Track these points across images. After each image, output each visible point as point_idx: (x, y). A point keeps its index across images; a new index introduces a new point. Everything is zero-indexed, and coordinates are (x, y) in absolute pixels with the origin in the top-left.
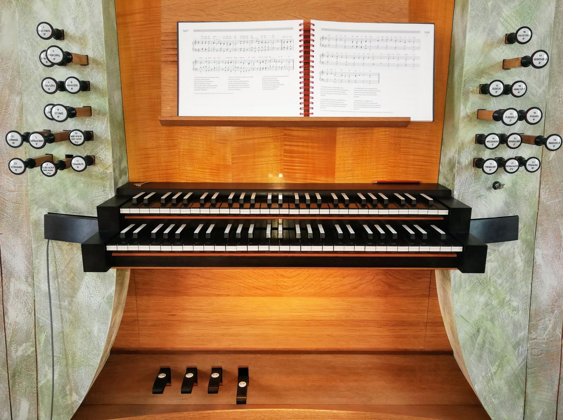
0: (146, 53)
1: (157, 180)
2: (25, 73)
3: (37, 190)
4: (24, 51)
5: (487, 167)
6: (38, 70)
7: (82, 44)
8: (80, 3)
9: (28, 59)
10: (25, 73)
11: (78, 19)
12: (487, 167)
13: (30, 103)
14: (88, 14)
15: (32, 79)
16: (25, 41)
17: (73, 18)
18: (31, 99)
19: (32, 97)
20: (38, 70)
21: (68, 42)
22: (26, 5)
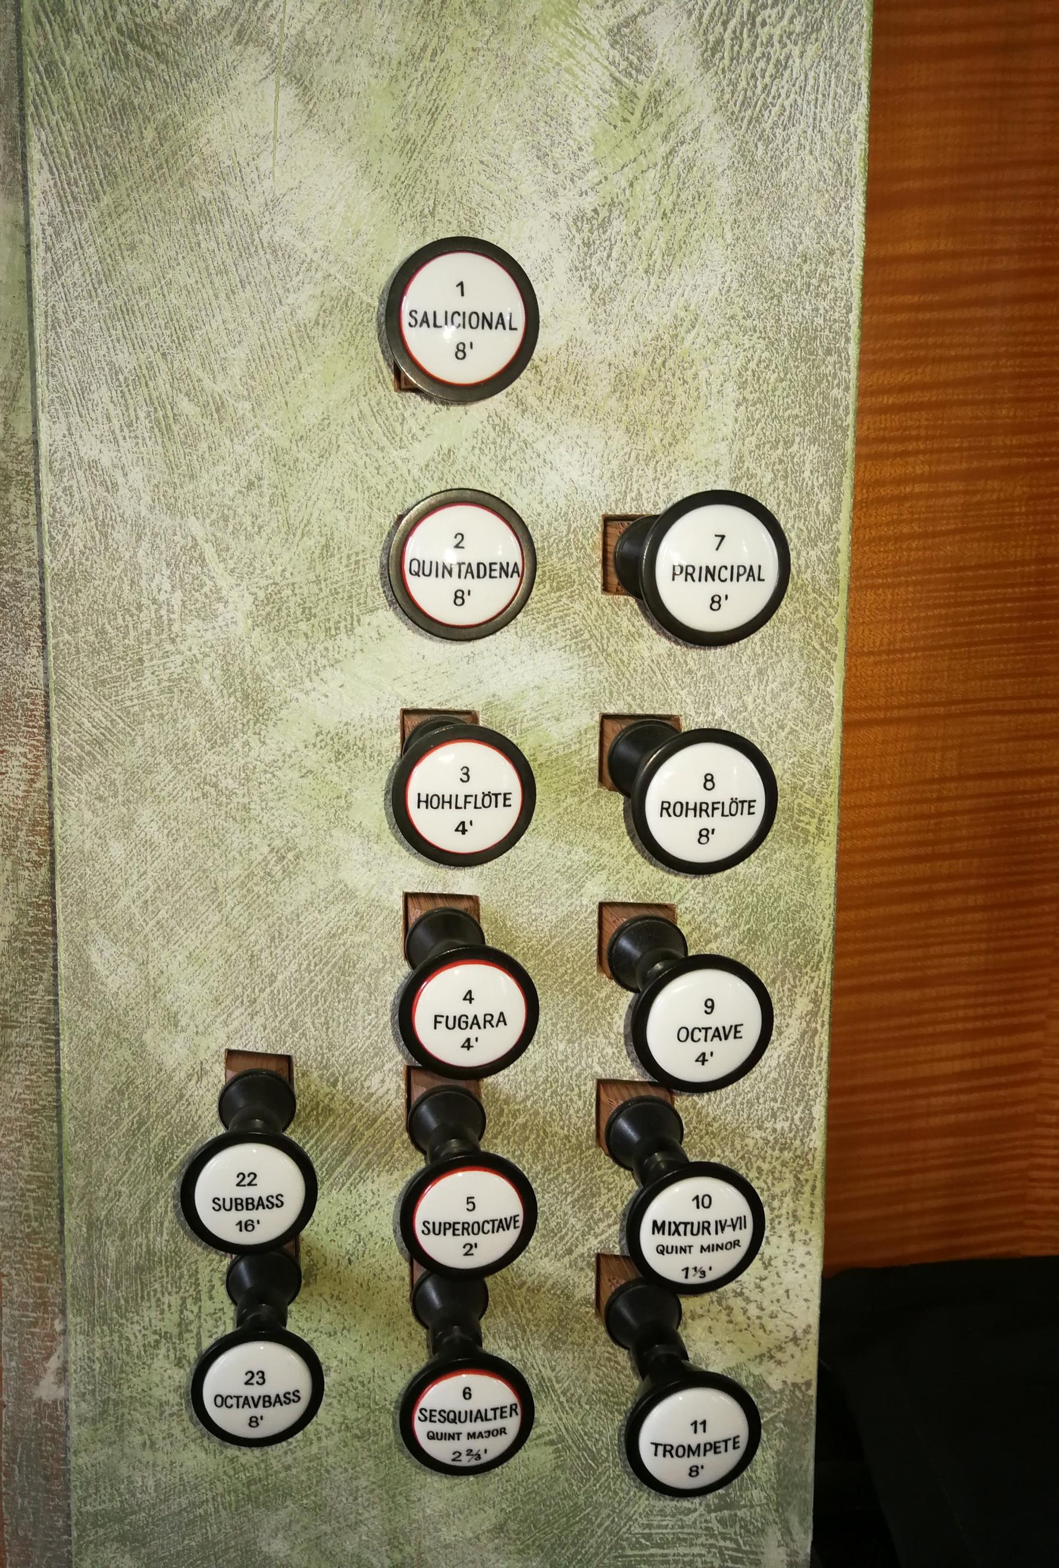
0: (932, 478)
1: (913, 1251)
2: (87, 634)
3: (147, 1455)
4: (93, 465)
5: (687, 572)
6: (206, 615)
7: (635, 429)
8: (655, 99)
9: (120, 535)
10: (87, 634)
11: (619, 226)
12: (687, 572)
13: (117, 849)
14: (724, 187)
15: (148, 682)
16: (102, 394)
17: (579, 218)
18: (127, 825)
19: (145, 814)
20: (206, 615)
21: (513, 414)
22: (125, 108)
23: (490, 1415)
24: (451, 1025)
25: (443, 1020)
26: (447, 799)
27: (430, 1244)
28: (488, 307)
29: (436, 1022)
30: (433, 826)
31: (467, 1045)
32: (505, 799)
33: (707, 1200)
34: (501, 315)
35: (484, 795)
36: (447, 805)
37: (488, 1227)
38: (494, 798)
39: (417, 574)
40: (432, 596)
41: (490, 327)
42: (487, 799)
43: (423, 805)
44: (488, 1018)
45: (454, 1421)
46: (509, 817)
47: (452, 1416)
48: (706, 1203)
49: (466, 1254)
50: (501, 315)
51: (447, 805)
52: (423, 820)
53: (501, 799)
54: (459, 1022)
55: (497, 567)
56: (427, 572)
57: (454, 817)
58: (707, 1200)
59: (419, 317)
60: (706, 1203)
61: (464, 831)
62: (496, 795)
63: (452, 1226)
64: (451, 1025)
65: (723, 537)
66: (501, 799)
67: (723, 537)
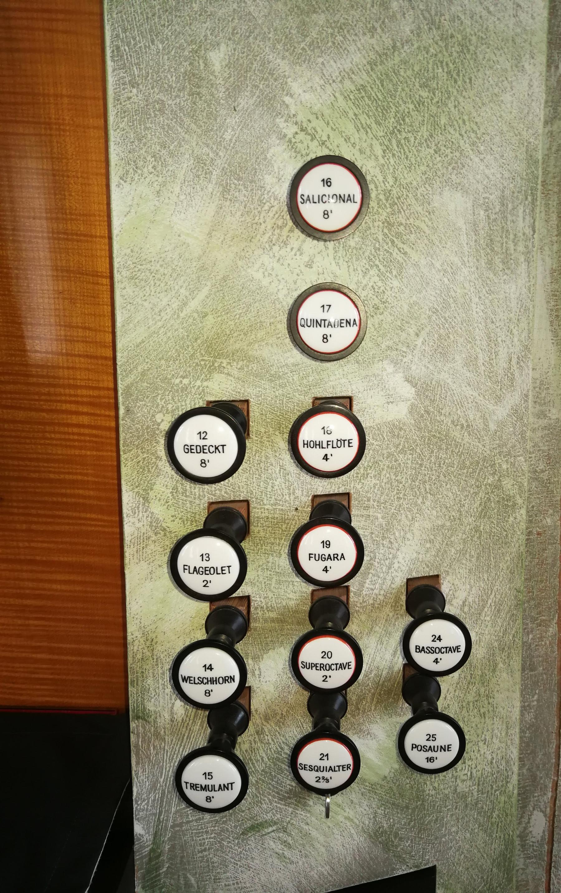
23: (337, 769)
24: (317, 559)
25: (313, 556)
26: (318, 443)
27: (308, 674)
28: (344, 191)
29: (310, 557)
30: (312, 457)
31: (326, 570)
32: (349, 443)
33: (329, 654)
34: (349, 195)
35: (338, 440)
36: (318, 446)
37: (334, 667)
38: (343, 442)
39: (303, 326)
40: (311, 337)
41: (344, 201)
42: (339, 442)
43: (306, 446)
44: (336, 556)
45: (317, 771)
46: (352, 452)
47: (316, 768)
48: (329, 656)
49: (324, 681)
50: (349, 195)
51: (318, 446)
52: (307, 454)
53: (346, 443)
54: (322, 558)
55: (345, 322)
56: (309, 324)
57: (321, 452)
58: (329, 654)
59: (305, 198)
60: (329, 656)
61: (327, 459)
62: (344, 441)
63: (316, 665)
64: (317, 559)
65: (330, 306)
66: (346, 443)
67: (330, 306)
